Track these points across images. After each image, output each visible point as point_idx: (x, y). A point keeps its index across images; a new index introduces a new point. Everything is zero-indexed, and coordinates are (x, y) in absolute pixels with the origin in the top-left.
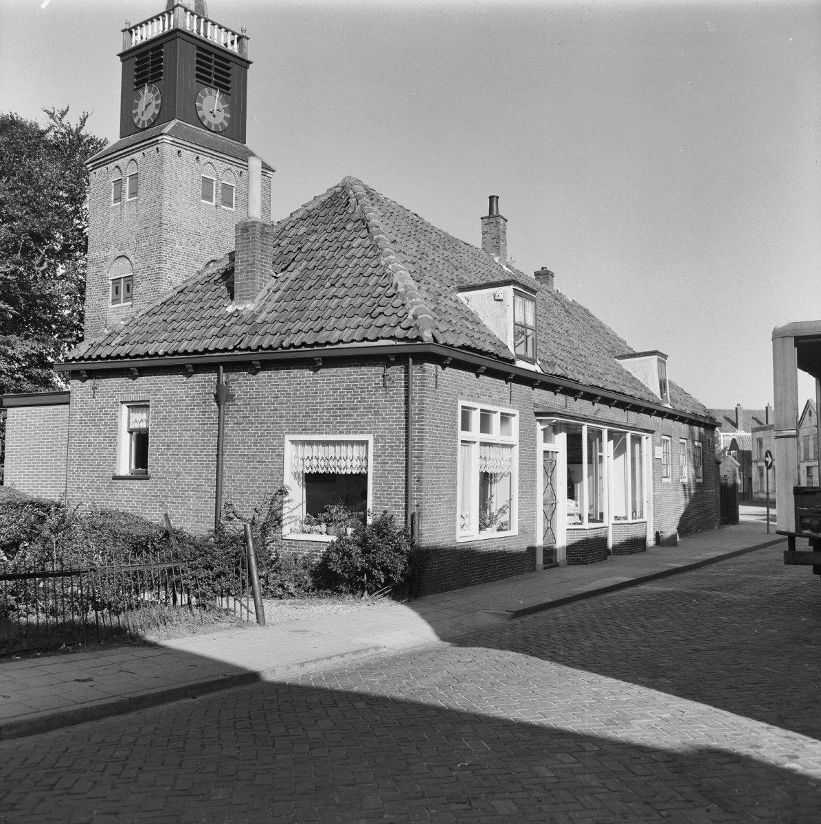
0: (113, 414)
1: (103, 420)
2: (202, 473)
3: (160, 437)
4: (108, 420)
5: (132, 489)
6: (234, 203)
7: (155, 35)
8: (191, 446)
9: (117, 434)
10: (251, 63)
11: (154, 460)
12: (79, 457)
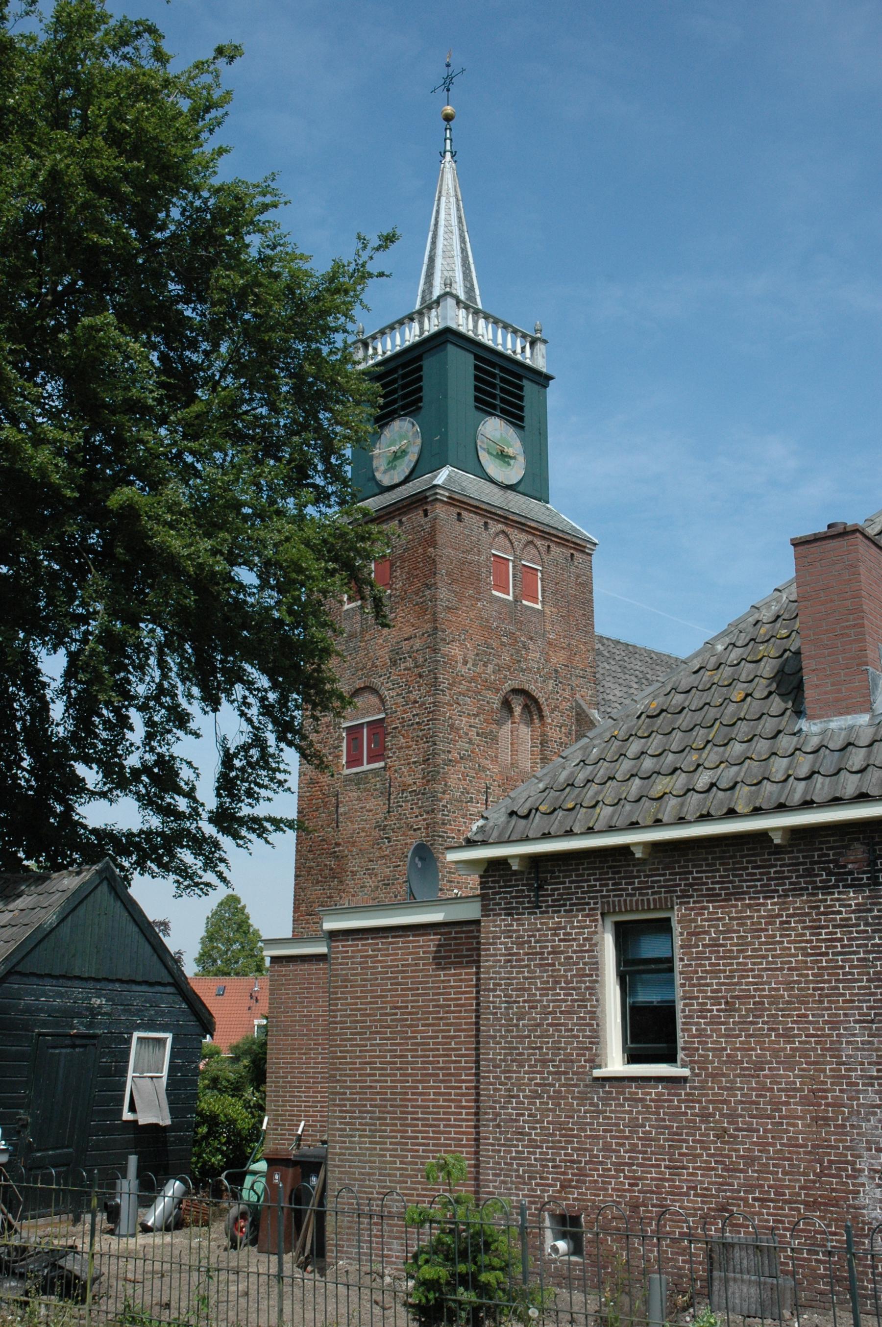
0: (585, 939)
1: (562, 952)
2: (823, 1063)
3: (707, 985)
4: (575, 952)
5: (642, 1100)
6: (540, 598)
7: (398, 348)
8: (788, 1003)
9: (596, 981)
10: (552, 378)
11: (694, 1036)
12: (507, 1031)
